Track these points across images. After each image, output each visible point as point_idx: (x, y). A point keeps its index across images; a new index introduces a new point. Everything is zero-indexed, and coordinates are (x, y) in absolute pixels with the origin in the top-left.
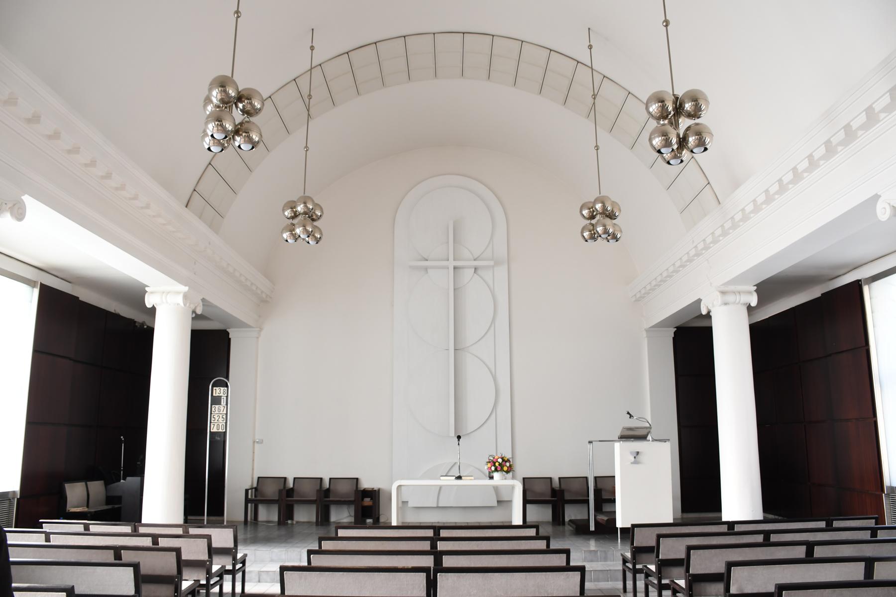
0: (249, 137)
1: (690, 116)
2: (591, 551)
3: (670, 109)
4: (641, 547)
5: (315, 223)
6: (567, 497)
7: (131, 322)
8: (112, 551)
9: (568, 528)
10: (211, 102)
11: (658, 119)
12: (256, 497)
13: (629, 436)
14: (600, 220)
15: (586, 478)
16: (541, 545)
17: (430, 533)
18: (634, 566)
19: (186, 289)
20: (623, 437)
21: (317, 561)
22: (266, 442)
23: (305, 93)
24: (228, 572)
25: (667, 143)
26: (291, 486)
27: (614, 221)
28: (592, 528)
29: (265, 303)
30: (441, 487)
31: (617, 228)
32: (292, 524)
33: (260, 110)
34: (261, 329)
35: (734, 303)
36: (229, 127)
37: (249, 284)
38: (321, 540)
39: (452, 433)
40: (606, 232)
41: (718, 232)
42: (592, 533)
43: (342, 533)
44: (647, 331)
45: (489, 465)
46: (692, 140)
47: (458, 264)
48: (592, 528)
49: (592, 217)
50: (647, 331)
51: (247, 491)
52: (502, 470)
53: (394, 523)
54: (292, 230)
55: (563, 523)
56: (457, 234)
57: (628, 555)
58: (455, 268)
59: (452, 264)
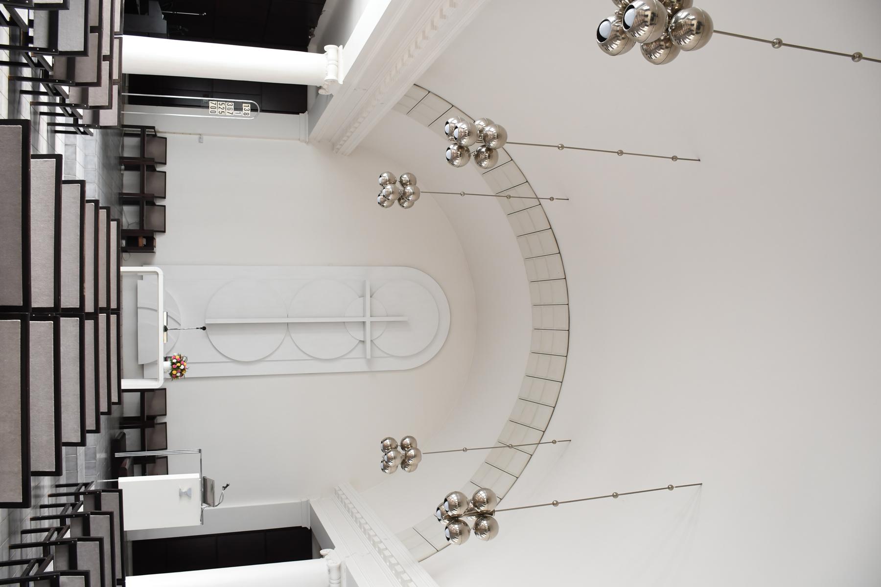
0: (457, 157)
1: (477, 525)
2: (95, 454)
3: (482, 508)
4: (100, 500)
5: (396, 201)
6: (148, 431)
7: (314, 24)
8: (97, 25)
9: (117, 432)
10: (487, 126)
11: (474, 499)
12: (147, 136)
13: (206, 487)
14: (401, 455)
15: (166, 449)
16: (104, 408)
17: (114, 305)
18: (68, 516)
19: (341, 82)
20: (204, 481)
21: (90, 208)
22: (200, 152)
23: (511, 193)
24: (76, 121)
25: (452, 507)
26: (158, 169)
27: (400, 466)
28: (117, 455)
29: (331, 147)
30: (156, 311)
31: (393, 469)
32: (121, 170)
33: (481, 166)
34: (307, 143)
35: (330, 579)
36: (464, 142)
37: (348, 134)
38: (108, 209)
39: (208, 321)
40: (389, 459)
41: (393, 561)
42: (112, 455)
43: (114, 225)
44: (308, 501)
45: (178, 357)
46: (456, 527)
47: (368, 325)
48: (117, 455)
49: (403, 447)
50: (308, 501)
51: (153, 128)
52: (173, 369)
53: (122, 269)
54: (391, 181)
55: (122, 428)
56: (397, 324)
57: (93, 488)
58: (364, 323)
59: (368, 320)
